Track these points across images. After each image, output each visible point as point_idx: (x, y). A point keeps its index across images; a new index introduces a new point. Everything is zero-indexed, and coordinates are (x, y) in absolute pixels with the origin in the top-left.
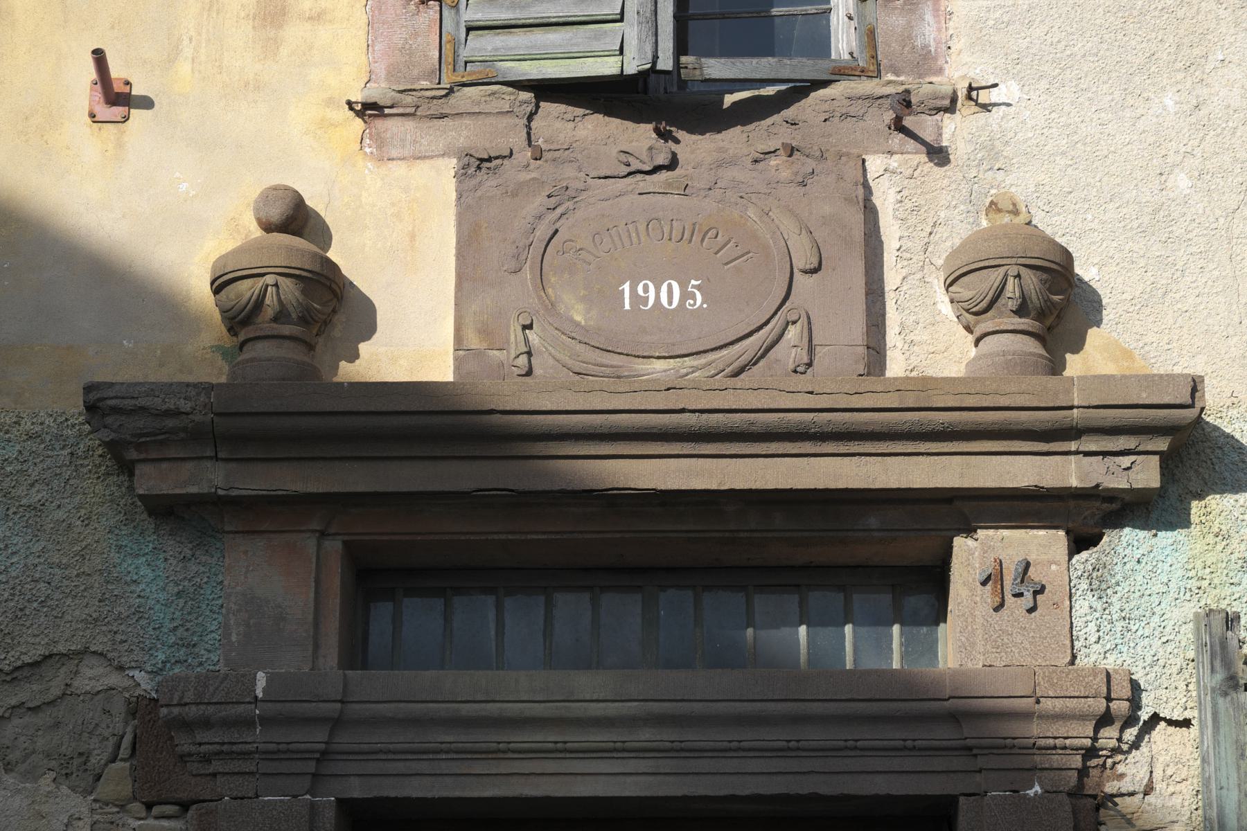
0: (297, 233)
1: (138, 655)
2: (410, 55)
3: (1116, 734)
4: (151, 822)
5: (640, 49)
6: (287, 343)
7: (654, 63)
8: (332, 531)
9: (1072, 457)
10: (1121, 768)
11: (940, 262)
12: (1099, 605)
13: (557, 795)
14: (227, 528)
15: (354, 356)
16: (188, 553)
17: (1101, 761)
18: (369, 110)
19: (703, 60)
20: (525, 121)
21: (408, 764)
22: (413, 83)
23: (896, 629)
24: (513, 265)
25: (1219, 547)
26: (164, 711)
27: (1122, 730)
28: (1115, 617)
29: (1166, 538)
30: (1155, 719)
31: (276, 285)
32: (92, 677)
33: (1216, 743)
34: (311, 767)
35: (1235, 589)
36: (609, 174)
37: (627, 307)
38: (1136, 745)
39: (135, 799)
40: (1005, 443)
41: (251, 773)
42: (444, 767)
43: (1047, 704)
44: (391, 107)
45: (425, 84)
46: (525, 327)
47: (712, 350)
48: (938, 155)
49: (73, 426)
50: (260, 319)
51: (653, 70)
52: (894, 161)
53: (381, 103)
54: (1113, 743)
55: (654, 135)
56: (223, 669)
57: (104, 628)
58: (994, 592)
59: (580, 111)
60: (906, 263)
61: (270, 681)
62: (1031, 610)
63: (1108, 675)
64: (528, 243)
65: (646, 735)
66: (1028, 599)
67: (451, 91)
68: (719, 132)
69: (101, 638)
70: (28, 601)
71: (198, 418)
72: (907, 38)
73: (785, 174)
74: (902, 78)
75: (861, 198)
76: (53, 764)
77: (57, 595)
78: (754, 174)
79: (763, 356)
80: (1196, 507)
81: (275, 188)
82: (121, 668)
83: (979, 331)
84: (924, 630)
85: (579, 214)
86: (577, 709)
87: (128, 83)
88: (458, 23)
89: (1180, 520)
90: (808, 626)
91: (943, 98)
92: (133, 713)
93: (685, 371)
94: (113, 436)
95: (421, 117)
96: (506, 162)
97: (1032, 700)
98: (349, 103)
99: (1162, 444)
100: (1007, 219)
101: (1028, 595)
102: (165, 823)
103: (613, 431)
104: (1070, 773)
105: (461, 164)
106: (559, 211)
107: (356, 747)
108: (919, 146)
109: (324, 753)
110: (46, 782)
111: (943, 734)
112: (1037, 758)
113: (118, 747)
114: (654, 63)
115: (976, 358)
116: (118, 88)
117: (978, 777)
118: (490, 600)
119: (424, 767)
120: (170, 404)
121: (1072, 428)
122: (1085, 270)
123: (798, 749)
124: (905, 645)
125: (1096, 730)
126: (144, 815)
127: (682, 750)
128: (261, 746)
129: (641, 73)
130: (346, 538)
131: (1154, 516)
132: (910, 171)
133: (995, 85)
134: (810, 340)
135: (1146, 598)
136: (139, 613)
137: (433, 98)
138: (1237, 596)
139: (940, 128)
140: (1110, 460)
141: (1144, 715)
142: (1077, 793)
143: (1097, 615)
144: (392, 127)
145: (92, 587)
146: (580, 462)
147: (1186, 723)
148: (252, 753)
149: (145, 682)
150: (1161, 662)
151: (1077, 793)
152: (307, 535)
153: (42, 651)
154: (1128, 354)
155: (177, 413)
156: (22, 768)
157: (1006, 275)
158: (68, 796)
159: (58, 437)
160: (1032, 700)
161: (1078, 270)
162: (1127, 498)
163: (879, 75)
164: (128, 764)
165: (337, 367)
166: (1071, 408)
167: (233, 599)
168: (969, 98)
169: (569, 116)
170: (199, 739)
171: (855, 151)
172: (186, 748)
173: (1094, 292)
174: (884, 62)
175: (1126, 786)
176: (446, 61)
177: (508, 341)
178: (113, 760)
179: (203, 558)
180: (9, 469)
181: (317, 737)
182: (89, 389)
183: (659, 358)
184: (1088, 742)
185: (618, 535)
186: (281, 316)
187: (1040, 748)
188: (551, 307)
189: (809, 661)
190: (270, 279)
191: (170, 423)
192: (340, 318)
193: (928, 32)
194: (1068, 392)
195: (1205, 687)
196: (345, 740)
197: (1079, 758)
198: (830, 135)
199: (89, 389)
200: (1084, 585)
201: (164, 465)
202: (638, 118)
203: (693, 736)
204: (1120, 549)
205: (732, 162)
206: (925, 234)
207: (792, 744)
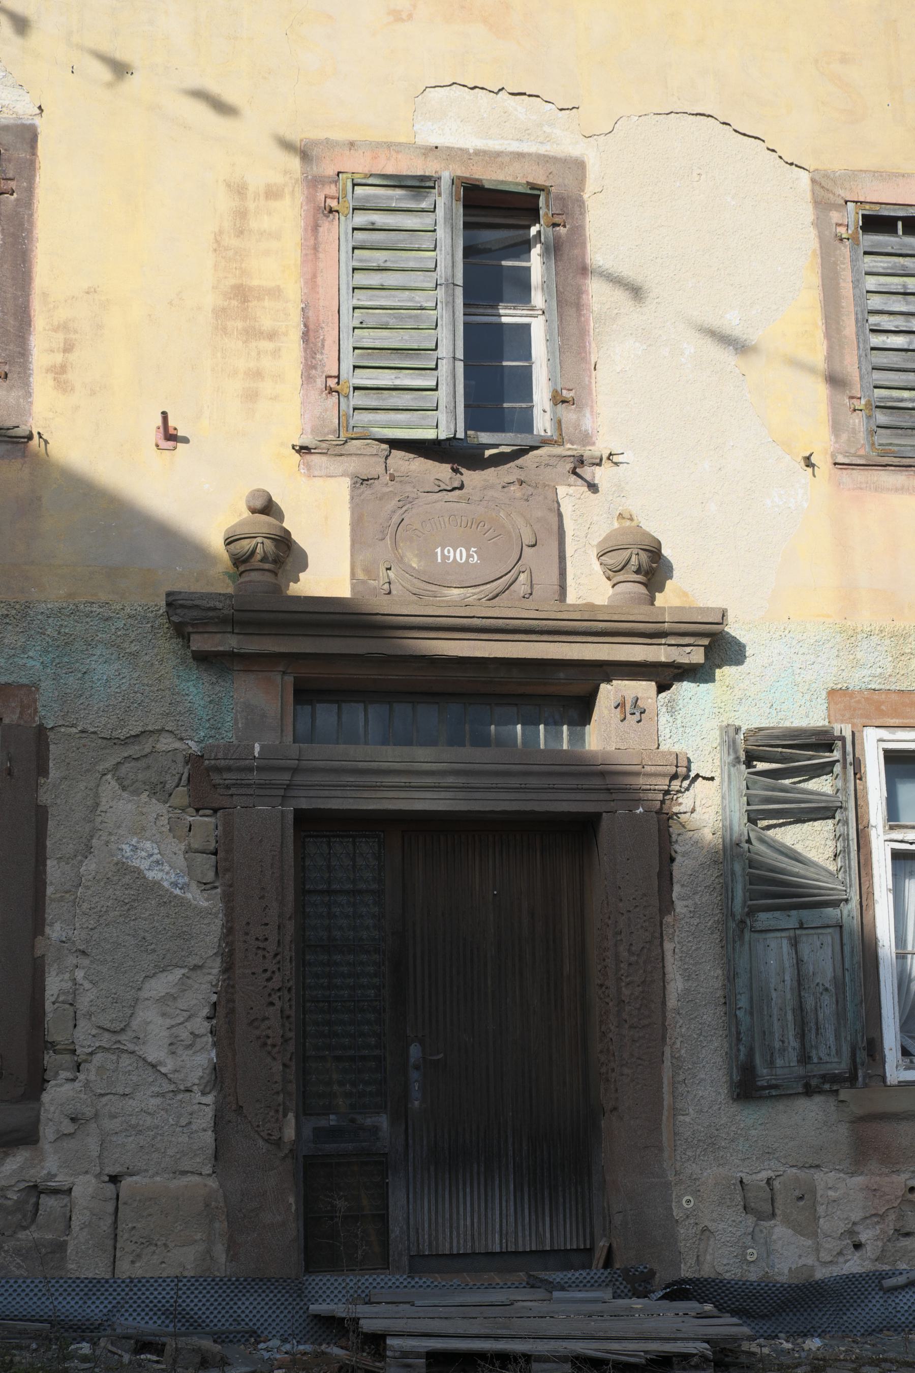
0: (268, 514)
1: (190, 733)
2: (323, 421)
3: (679, 784)
4: (198, 818)
5: (448, 427)
6: (267, 573)
7: (455, 434)
8: (289, 671)
9: (662, 647)
10: (680, 800)
11: (595, 543)
12: (671, 720)
13: (405, 809)
14: (235, 669)
15: (297, 580)
16: (214, 680)
17: (671, 796)
18: (303, 450)
19: (479, 433)
20: (384, 459)
21: (331, 792)
22: (325, 437)
23: (565, 728)
24: (381, 537)
25: (729, 693)
26: (207, 762)
27: (682, 782)
28: (679, 726)
29: (704, 687)
30: (697, 776)
31: (263, 543)
32: (166, 743)
33: (730, 789)
34: (282, 792)
35: (735, 713)
36: (429, 490)
37: (439, 560)
38: (687, 789)
39: (190, 806)
40: (630, 638)
41: (251, 795)
42: (349, 794)
43: (648, 769)
44: (315, 449)
45: (331, 437)
46: (387, 569)
47: (483, 584)
48: (593, 487)
49: (152, 612)
50: (253, 560)
51: (454, 438)
52: (571, 490)
53: (310, 447)
54: (678, 788)
55: (450, 470)
56: (236, 742)
57: (172, 718)
58: (621, 712)
59: (412, 456)
60: (576, 543)
61: (262, 748)
62: (639, 722)
63: (677, 755)
64: (388, 524)
65: (450, 780)
66: (637, 717)
67: (346, 442)
68: (483, 470)
69: (170, 723)
70: (132, 703)
71: (225, 612)
72: (577, 426)
73: (518, 495)
74: (575, 447)
75: (556, 508)
76: (147, 787)
77: (147, 700)
78: (503, 494)
79: (508, 589)
80: (718, 672)
81: (258, 490)
82: (181, 739)
83: (615, 580)
84: (579, 728)
85: (414, 511)
87: (175, 429)
88: (348, 406)
89: (710, 679)
90: (545, 725)
91: (596, 458)
92: (187, 763)
93: (469, 595)
94: (180, 619)
95: (330, 455)
96: (376, 481)
97: (641, 766)
98: (293, 447)
99: (706, 642)
100: (628, 523)
101: (638, 714)
102: (206, 819)
103: (438, 626)
104: (657, 802)
105: (353, 482)
106: (404, 509)
107: (305, 783)
108: (584, 482)
109: (288, 785)
110: (144, 797)
111: (597, 782)
112: (641, 795)
113: (180, 779)
114: (455, 434)
115: (614, 595)
116: (171, 431)
117: (612, 804)
118: (361, 706)
119: (339, 793)
120: (211, 604)
121: (664, 632)
122: (665, 551)
123: (525, 788)
124: (571, 735)
125: (670, 782)
126: (195, 814)
127: (468, 788)
128: (257, 781)
129: (448, 439)
130: (295, 675)
131: (698, 676)
132: (579, 495)
133: (623, 454)
134: (531, 582)
135: (694, 717)
136: (190, 711)
137: (337, 445)
138: (737, 717)
139: (594, 474)
140: (680, 648)
141: (692, 774)
142: (659, 812)
143: (670, 724)
144: (315, 459)
145: (165, 697)
146: (419, 640)
147: (712, 779)
148: (252, 784)
149: (194, 747)
150: (701, 749)
151: (659, 812)
152: (276, 673)
153: (140, 729)
154: (685, 594)
155: (215, 609)
156: (131, 789)
157: (632, 553)
158: (156, 804)
159: (145, 617)
160: (641, 766)
161: (663, 552)
162: (686, 667)
163: (563, 445)
164: (186, 789)
165: (288, 586)
166: (664, 622)
167: (239, 705)
168: (609, 458)
169: (406, 458)
170: (225, 777)
171: (552, 484)
172: (217, 782)
173: (669, 562)
174: (566, 438)
175: (682, 809)
176: (343, 426)
177: (378, 576)
178: (177, 786)
179: (222, 684)
180: (119, 633)
181: (285, 777)
182: (168, 594)
183: (455, 587)
184: (666, 787)
185: (434, 678)
186: (264, 559)
187: (643, 790)
188: (401, 559)
189: (524, 743)
190: (259, 540)
191: (211, 614)
192: (290, 559)
193: (588, 423)
194: (663, 614)
195: (725, 762)
196: (299, 779)
197: (661, 795)
198: (540, 475)
199: (168, 594)
200: (664, 709)
201: (206, 635)
202: (442, 460)
203: (474, 781)
204: (681, 692)
205: (492, 487)
206: (586, 528)
207: (523, 786)
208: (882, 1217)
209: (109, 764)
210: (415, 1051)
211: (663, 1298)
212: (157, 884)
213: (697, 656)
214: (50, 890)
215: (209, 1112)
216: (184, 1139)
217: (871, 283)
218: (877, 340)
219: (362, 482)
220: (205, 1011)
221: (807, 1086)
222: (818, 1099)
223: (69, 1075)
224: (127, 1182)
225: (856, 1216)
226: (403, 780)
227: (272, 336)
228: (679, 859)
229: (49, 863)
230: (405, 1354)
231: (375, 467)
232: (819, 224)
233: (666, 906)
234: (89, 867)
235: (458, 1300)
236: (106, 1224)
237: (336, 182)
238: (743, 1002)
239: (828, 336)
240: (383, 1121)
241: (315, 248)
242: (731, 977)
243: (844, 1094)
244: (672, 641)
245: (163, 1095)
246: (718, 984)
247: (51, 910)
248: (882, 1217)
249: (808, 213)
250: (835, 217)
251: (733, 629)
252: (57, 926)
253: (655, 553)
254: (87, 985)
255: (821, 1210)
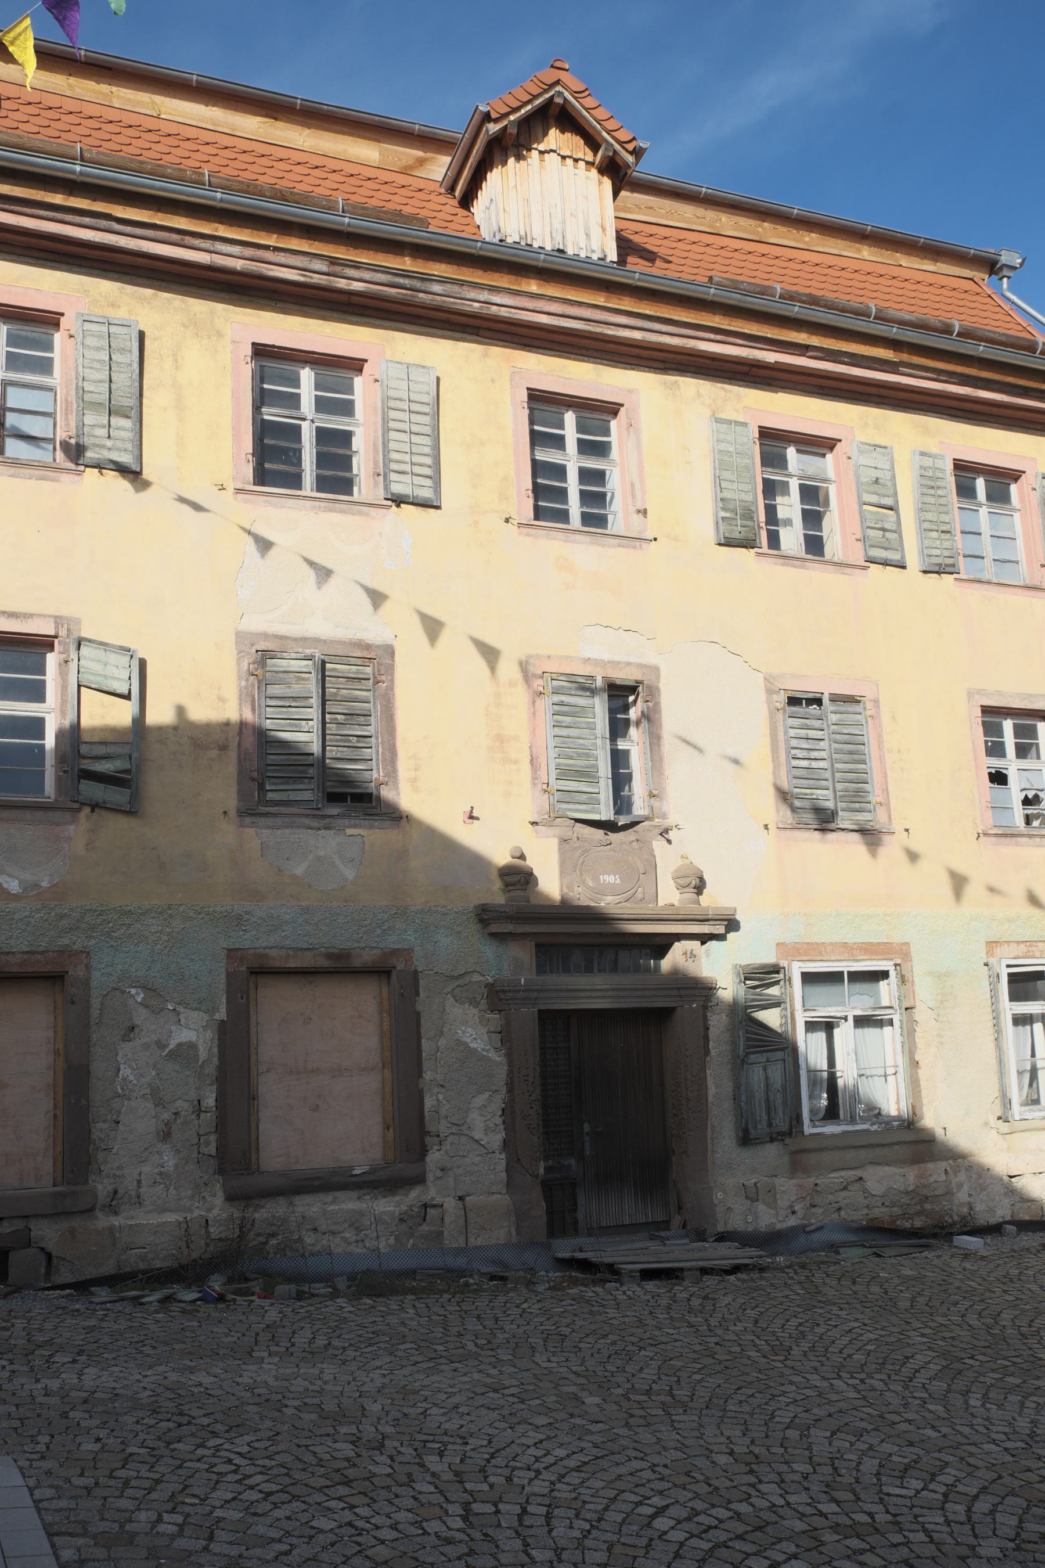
18: (534, 823)
48: (669, 841)
65: (610, 993)
72: (660, 809)
86: (595, 987)
110: (467, 1005)
149: (490, 980)
181: (535, 995)
188: (584, 882)
193: (665, 809)
208: (804, 1198)
209: (449, 989)
210: (586, 1127)
211: (715, 1241)
212: (476, 1049)
213: (720, 930)
214: (424, 1055)
215: (504, 1163)
216: (492, 1176)
217: (792, 732)
218: (795, 763)
219: (564, 841)
220: (500, 1113)
221: (771, 1138)
222: (776, 1143)
223: (438, 1147)
224: (468, 1199)
225: (793, 1198)
226: (588, 994)
227: (516, 762)
228: (711, 1029)
229: (423, 1041)
230: (631, 1271)
231: (568, 834)
232: (769, 701)
233: (707, 1052)
234: (442, 1042)
235: (630, 1246)
236: (462, 1221)
237: (542, 677)
238: (744, 1098)
239: (773, 761)
240: (573, 1162)
241: (534, 714)
242: (737, 1087)
243: (787, 1141)
244: (711, 923)
245: (481, 1155)
246: (731, 1090)
247: (426, 1065)
248: (804, 1198)
249: (762, 695)
250: (775, 697)
251: (738, 917)
252: (429, 1073)
253: (701, 879)
254: (445, 1102)
255: (778, 1196)
